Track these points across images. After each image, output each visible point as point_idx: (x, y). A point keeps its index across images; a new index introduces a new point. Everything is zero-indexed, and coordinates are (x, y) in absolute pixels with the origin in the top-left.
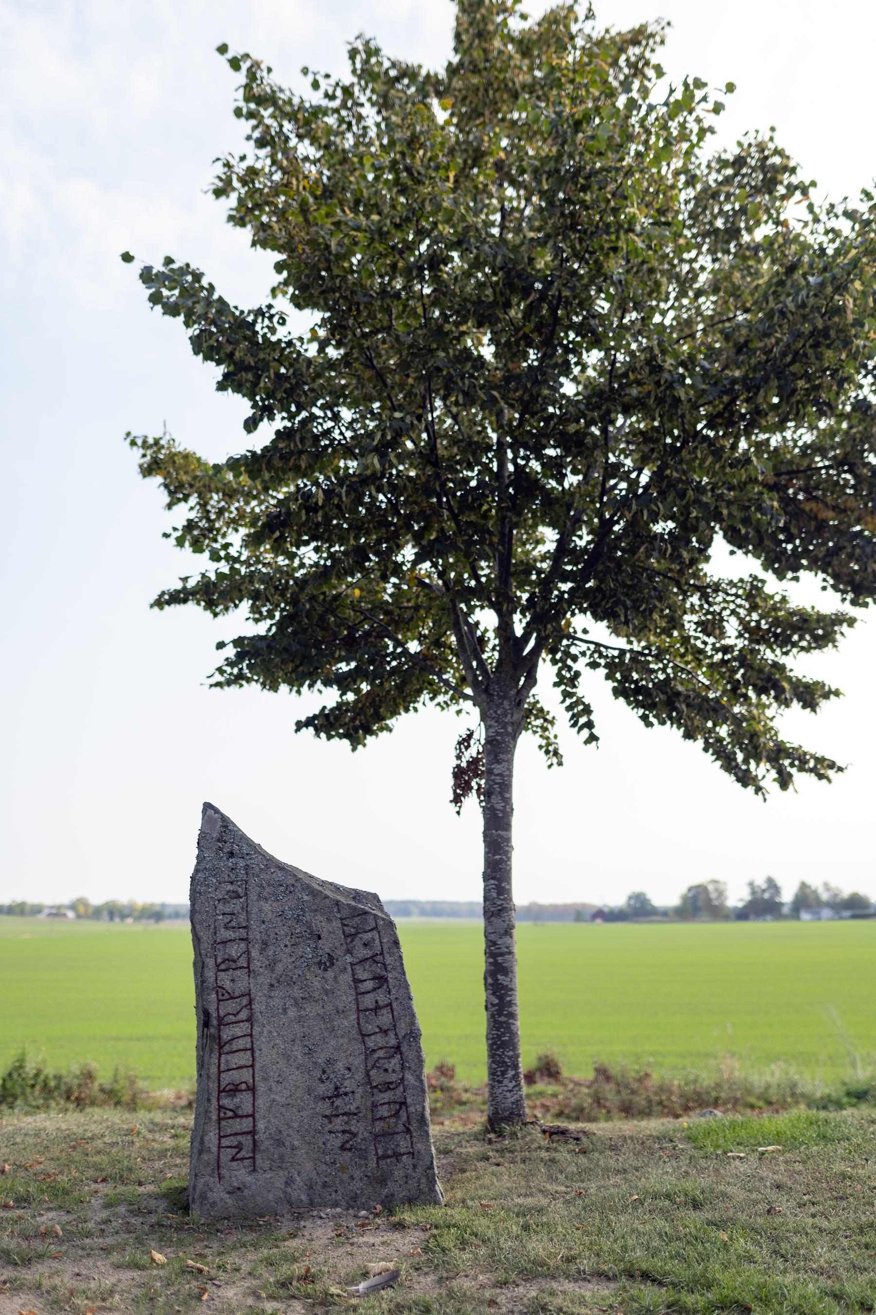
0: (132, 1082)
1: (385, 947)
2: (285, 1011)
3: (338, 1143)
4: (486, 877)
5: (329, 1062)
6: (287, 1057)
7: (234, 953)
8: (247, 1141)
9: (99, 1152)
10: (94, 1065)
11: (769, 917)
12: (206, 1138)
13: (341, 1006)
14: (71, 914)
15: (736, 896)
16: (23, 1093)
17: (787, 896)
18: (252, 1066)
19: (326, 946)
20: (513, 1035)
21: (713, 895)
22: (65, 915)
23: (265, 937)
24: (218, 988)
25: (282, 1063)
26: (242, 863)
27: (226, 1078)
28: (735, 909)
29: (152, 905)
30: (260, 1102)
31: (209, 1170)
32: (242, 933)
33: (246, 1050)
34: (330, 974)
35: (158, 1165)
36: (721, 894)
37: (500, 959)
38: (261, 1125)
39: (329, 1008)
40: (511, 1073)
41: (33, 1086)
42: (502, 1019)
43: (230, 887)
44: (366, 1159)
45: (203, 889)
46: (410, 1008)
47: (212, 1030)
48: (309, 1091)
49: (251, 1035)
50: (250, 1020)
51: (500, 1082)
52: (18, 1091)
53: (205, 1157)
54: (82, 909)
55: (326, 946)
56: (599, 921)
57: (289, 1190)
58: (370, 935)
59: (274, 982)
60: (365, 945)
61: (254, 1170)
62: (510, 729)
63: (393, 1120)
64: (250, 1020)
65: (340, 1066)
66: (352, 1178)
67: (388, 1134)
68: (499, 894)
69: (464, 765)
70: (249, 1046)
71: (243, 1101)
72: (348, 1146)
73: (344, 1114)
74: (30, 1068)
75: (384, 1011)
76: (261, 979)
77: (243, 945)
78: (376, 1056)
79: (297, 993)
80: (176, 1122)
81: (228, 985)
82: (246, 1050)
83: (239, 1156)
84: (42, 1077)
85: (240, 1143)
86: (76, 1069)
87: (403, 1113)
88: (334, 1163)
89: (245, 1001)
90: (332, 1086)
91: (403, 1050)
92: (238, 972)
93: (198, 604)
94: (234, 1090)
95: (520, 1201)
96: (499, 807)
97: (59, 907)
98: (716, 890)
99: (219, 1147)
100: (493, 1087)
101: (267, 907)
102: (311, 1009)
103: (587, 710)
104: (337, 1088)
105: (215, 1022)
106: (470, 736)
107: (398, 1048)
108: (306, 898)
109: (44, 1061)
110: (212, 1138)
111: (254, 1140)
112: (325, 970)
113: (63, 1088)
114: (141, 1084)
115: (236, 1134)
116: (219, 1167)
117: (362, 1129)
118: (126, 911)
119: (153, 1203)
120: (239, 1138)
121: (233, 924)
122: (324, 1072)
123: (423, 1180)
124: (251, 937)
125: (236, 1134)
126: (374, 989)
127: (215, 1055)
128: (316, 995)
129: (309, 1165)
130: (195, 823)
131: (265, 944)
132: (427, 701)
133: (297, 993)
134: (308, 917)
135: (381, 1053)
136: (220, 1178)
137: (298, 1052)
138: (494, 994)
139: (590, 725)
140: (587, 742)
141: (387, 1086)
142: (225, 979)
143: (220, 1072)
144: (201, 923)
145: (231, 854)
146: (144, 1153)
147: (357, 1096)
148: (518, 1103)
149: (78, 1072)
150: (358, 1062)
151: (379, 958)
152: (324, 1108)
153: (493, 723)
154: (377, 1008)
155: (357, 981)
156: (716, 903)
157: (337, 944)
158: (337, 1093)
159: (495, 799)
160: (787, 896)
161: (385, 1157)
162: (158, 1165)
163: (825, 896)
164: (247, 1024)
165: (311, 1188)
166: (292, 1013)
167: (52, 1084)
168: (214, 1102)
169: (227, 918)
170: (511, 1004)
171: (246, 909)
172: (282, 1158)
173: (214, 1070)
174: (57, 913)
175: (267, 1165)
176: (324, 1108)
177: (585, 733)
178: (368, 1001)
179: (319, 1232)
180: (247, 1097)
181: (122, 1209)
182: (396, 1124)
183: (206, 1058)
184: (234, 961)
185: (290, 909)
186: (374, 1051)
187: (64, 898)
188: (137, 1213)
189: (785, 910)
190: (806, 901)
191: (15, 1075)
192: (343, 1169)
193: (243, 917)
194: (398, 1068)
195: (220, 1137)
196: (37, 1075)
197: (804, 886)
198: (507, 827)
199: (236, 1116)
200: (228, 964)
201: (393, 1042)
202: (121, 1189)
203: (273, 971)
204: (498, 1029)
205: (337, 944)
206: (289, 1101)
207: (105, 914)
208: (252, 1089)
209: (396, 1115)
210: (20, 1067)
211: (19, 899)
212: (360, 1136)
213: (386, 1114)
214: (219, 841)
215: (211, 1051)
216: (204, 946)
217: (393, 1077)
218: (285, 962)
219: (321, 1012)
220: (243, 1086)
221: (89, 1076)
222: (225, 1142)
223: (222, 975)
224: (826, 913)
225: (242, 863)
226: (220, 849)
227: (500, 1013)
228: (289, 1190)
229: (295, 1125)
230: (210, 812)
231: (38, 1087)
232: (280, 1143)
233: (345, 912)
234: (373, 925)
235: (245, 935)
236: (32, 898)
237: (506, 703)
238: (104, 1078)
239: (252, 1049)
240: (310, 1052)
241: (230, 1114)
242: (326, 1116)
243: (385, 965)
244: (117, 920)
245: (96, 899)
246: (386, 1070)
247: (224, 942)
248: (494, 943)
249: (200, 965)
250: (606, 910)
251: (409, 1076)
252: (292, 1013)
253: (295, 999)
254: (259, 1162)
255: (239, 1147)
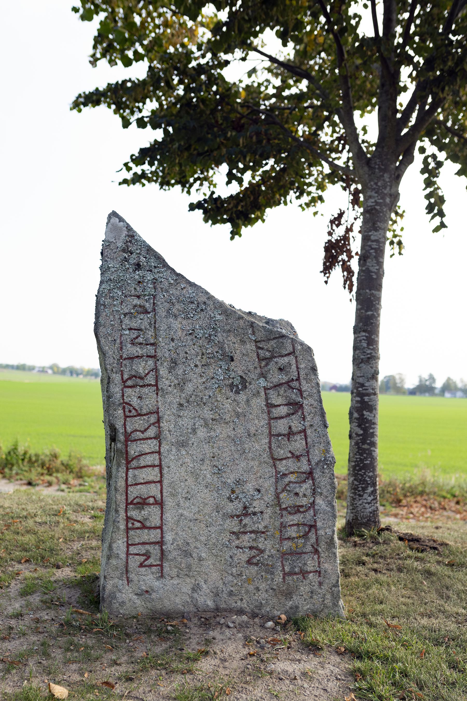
0: (80, 461)
1: (302, 373)
2: (194, 431)
3: (245, 557)
4: (356, 330)
5: (238, 482)
6: (195, 475)
7: (141, 370)
8: (155, 551)
9: (28, 532)
10: (57, 450)
11: (427, 394)
12: (114, 545)
13: (253, 430)
14: (50, 371)
15: (411, 383)
16: (17, 463)
17: (439, 384)
18: (161, 482)
19: (238, 368)
20: (373, 459)
21: (398, 381)
22: (47, 372)
23: (174, 356)
24: (125, 404)
25: (190, 481)
26: (149, 277)
27: (134, 492)
28: (409, 389)
29: (93, 369)
30: (168, 516)
31: (118, 573)
32: (150, 350)
33: (154, 466)
34: (242, 397)
35: (77, 546)
36: (402, 381)
37: (366, 399)
38: (169, 537)
39: (240, 431)
40: (370, 489)
41: (23, 460)
42: (366, 446)
43: (136, 301)
44: (272, 573)
45: (108, 301)
46: (325, 435)
47: (119, 445)
48: (218, 509)
49: (159, 453)
50: (158, 437)
51: (360, 496)
52: (14, 461)
53: (114, 562)
54: (56, 369)
55: (238, 368)
56: (333, 391)
57: (195, 595)
58: (286, 359)
59: (183, 401)
60: (280, 369)
61: (162, 576)
62: (388, 200)
63: (301, 541)
64: (158, 437)
65: (250, 487)
66: (258, 589)
67: (297, 553)
68: (369, 344)
69: (333, 240)
70: (157, 463)
71: (152, 514)
72: (255, 561)
73: (251, 532)
74: (21, 450)
75: (298, 437)
76: (169, 398)
77: (151, 362)
78: (287, 480)
79: (207, 414)
80: (95, 505)
81: (135, 402)
82: (154, 466)
83: (146, 563)
84: (28, 456)
85: (148, 551)
86: (47, 452)
87: (312, 535)
88: (241, 575)
89: (153, 419)
90: (241, 506)
91: (316, 476)
92: (146, 390)
93: (109, 107)
94: (142, 503)
95: (424, 621)
96: (373, 269)
97: (43, 368)
98: (400, 378)
99: (128, 554)
100: (354, 499)
101: (176, 324)
102: (222, 431)
103: (441, 200)
104: (245, 508)
105: (122, 438)
106: (341, 215)
107: (310, 474)
108: (218, 317)
109: (29, 447)
110: (120, 545)
111: (162, 550)
112: (237, 392)
113: (40, 462)
114: (84, 462)
115: (144, 543)
116: (127, 571)
117: (269, 547)
118: (79, 372)
119: (65, 594)
120: (147, 547)
121: (140, 340)
122: (233, 492)
123: (328, 596)
124: (159, 354)
125: (144, 543)
126: (288, 415)
127: (122, 470)
128: (227, 417)
129: (215, 575)
130: (98, 234)
131: (174, 362)
132: (294, 200)
133: (207, 414)
134: (220, 337)
135: (292, 478)
136: (129, 581)
137: (207, 471)
138: (359, 426)
139: (441, 214)
140: (436, 230)
141: (297, 509)
142: (132, 395)
143: (127, 486)
144: (106, 337)
145: (138, 266)
146: (67, 533)
147: (266, 516)
148: (375, 513)
149: (48, 453)
150: (268, 484)
151: (295, 384)
152: (233, 524)
153: (373, 194)
154: (290, 434)
155: (270, 406)
156: (399, 385)
157: (251, 367)
158: (247, 511)
159: (370, 263)
160: (439, 384)
161: (291, 573)
162: (77, 546)
163: (460, 385)
164: (155, 442)
165: (217, 595)
166: (202, 433)
167: (34, 459)
168: (122, 514)
169: (134, 334)
170: (373, 435)
171: (154, 325)
172: (189, 567)
173: (121, 483)
174: (43, 371)
175: (174, 572)
176: (233, 524)
177: (438, 219)
178: (281, 426)
179: (230, 648)
180: (156, 510)
181: (35, 599)
182: (304, 545)
183: (114, 471)
184: (142, 378)
185: (201, 328)
186: (285, 475)
187: (47, 363)
188: (49, 604)
189: (437, 391)
190: (449, 387)
191: (12, 453)
192: (249, 580)
193: (150, 333)
194: (309, 492)
195: (128, 545)
196: (25, 453)
197: (449, 379)
198: (379, 287)
199: (144, 527)
200: (136, 381)
201: (305, 467)
202: (41, 571)
203: (182, 390)
204: (361, 454)
205: (251, 367)
206: (197, 516)
207: (68, 373)
208: (160, 504)
209: (305, 536)
210: (15, 449)
211: (22, 362)
212: (267, 553)
213: (294, 535)
214: (124, 251)
215: (119, 465)
216: (110, 360)
217: (304, 501)
218: (195, 382)
219: (232, 434)
220: (151, 500)
221: (55, 456)
222: (133, 550)
223: (129, 391)
224: (459, 394)
225: (149, 277)
226: (126, 260)
227: (364, 441)
228: (195, 595)
229: (203, 539)
230: (115, 220)
231: (26, 460)
232: (187, 554)
233: (260, 335)
234: (290, 349)
235: (152, 353)
236: (29, 362)
237: (386, 176)
238: (63, 457)
239: (160, 466)
240: (219, 472)
241: (138, 525)
242: (233, 533)
243: (300, 391)
244: (75, 375)
245: (63, 365)
246: (297, 494)
247: (131, 359)
248: (362, 385)
249: (106, 382)
250: (338, 385)
251: (319, 501)
252: (202, 433)
253: (205, 420)
254: (166, 570)
255: (147, 555)
